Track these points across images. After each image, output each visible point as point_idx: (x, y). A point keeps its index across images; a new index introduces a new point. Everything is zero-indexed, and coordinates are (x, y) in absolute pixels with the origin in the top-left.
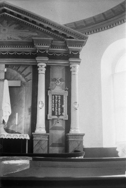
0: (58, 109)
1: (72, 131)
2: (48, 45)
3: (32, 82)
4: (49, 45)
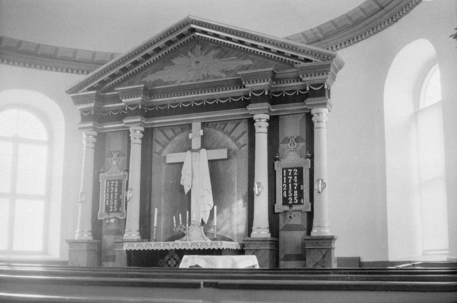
0: (293, 193)
2: (266, 80)
4: (268, 81)
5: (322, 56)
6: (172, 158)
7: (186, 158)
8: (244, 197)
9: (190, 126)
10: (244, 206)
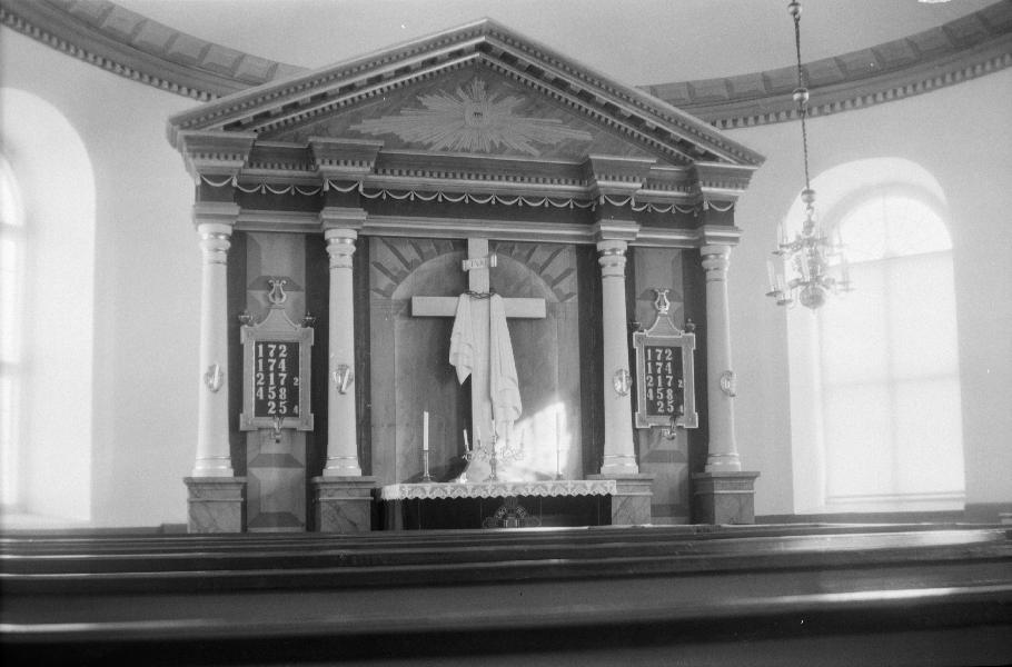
1: (716, 466)
2: (638, 178)
3: (577, 300)
5: (740, 154)
6: (427, 306)
9: (461, 245)
10: (574, 414)
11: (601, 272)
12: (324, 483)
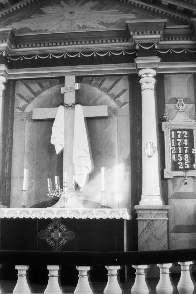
0: (183, 156)
7: (60, 114)
8: (126, 160)
9: (62, 80)
10: (127, 170)
11: (141, 88)
12: (141, 209)
